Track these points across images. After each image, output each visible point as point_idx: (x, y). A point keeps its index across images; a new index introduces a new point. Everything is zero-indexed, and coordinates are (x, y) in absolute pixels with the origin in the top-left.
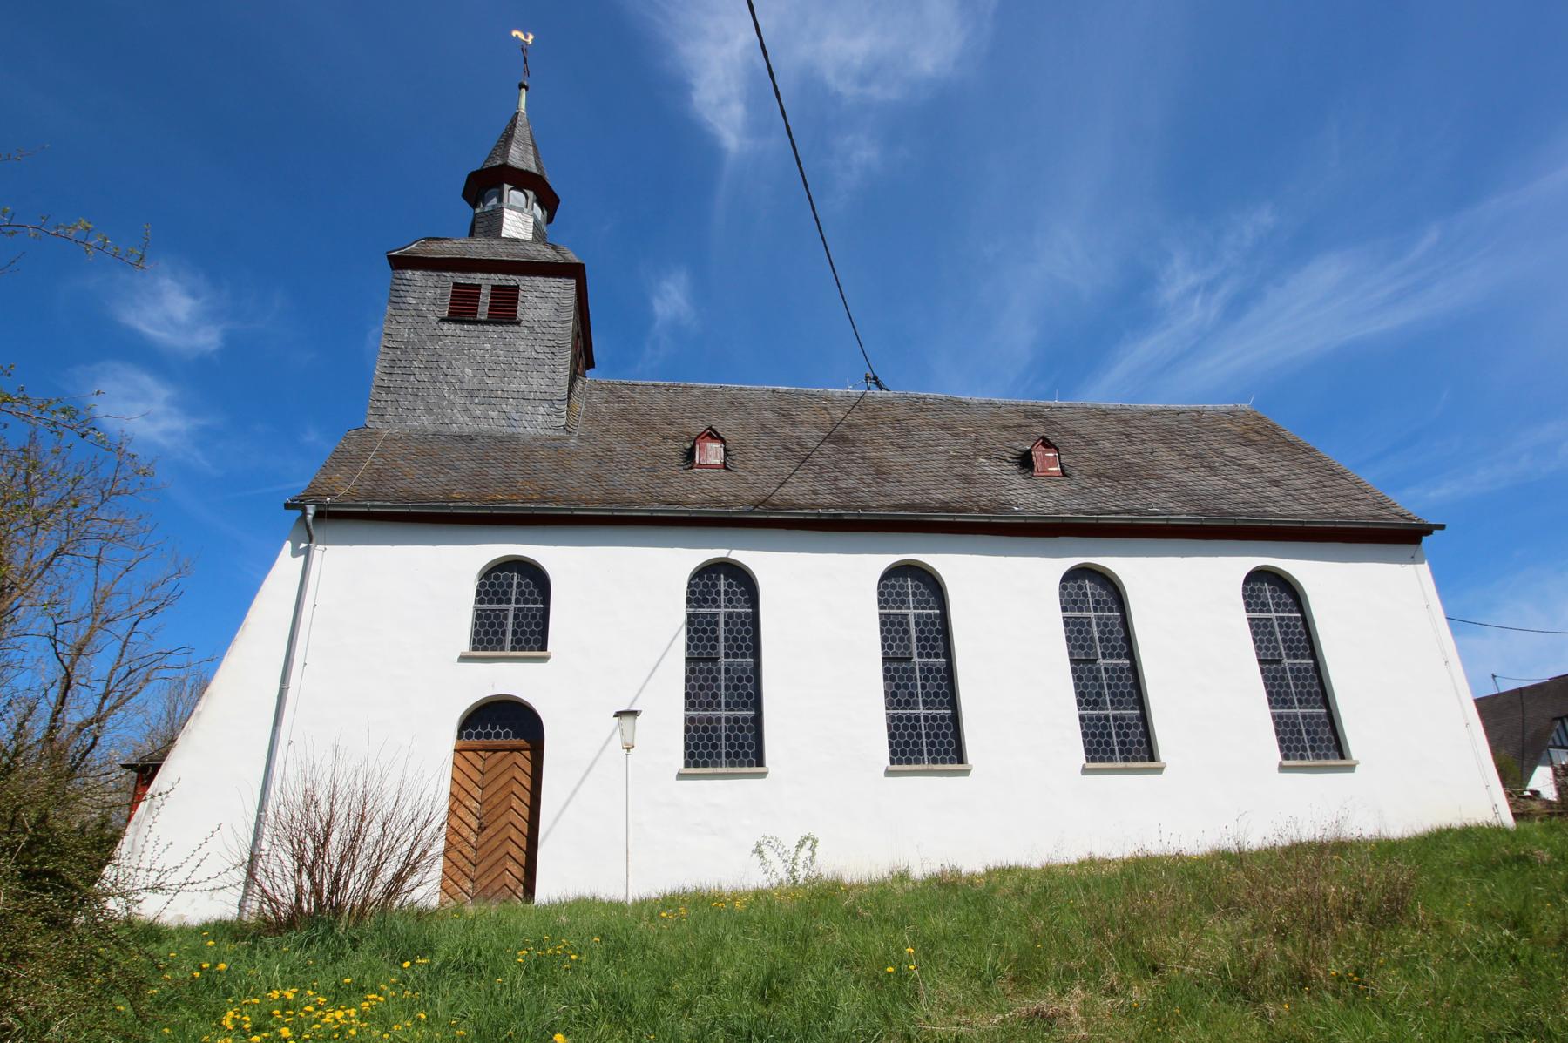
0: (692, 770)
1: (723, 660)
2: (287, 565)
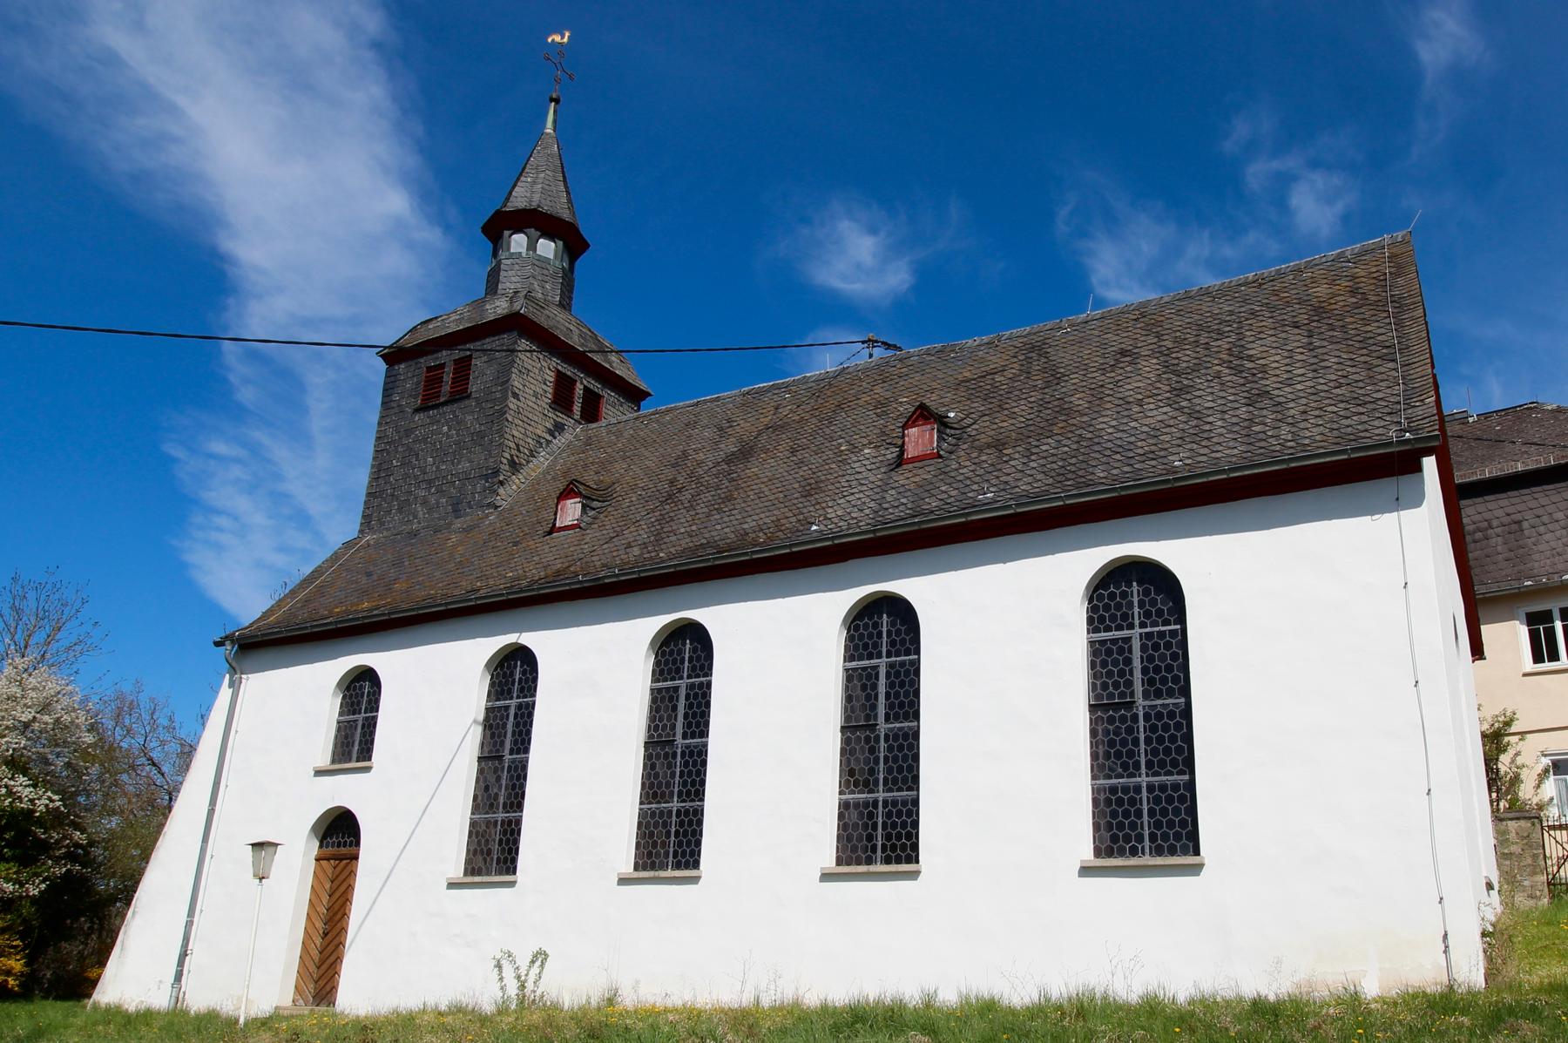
0: (470, 879)
2: (225, 693)
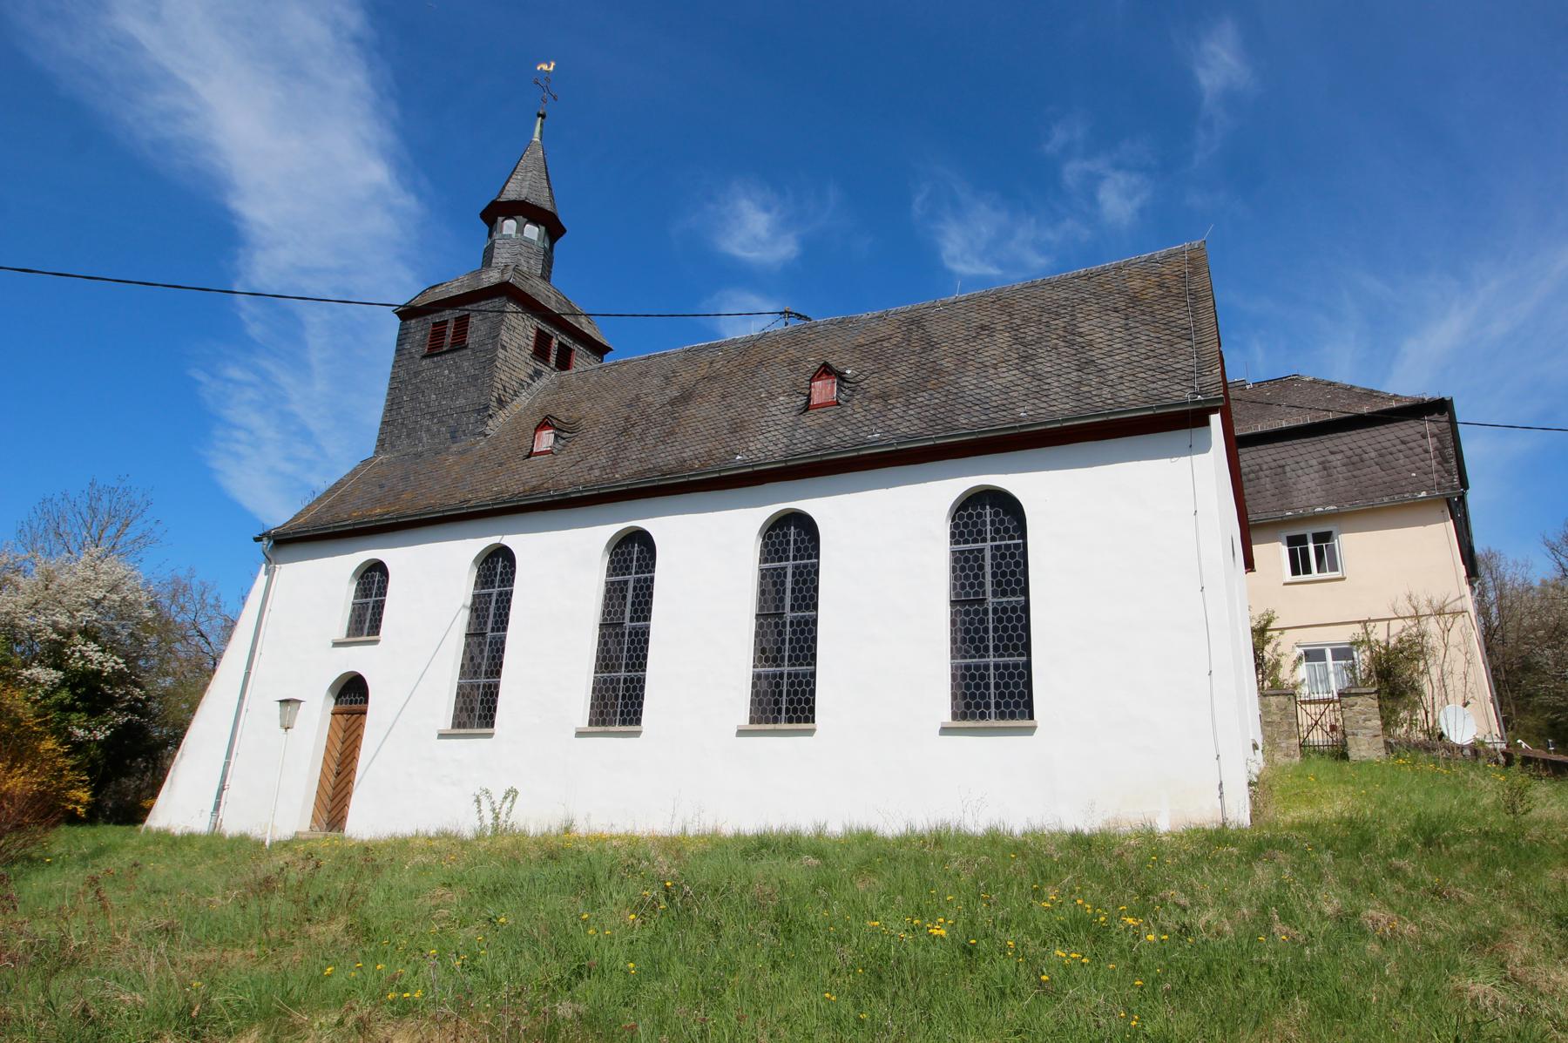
1: (489, 634)
2: (262, 579)
